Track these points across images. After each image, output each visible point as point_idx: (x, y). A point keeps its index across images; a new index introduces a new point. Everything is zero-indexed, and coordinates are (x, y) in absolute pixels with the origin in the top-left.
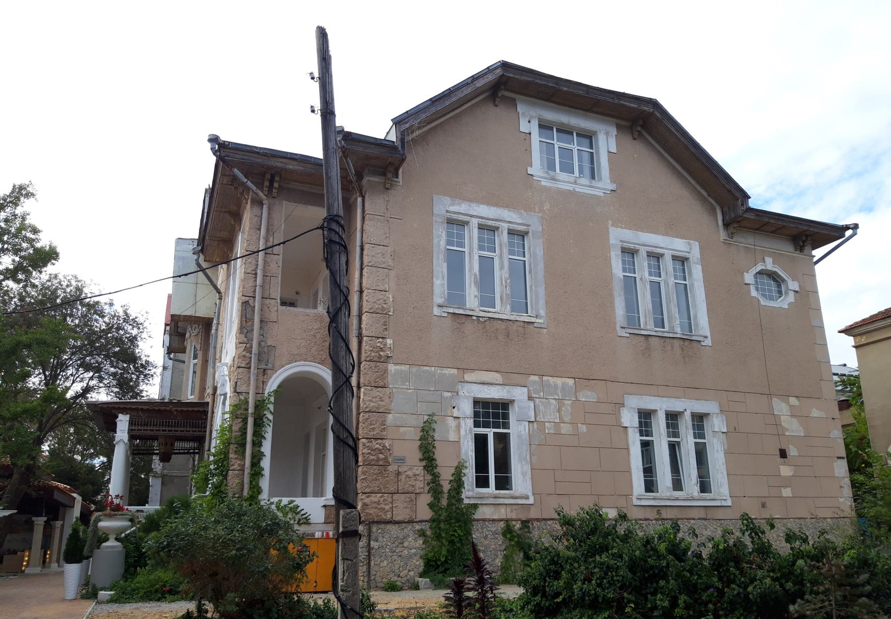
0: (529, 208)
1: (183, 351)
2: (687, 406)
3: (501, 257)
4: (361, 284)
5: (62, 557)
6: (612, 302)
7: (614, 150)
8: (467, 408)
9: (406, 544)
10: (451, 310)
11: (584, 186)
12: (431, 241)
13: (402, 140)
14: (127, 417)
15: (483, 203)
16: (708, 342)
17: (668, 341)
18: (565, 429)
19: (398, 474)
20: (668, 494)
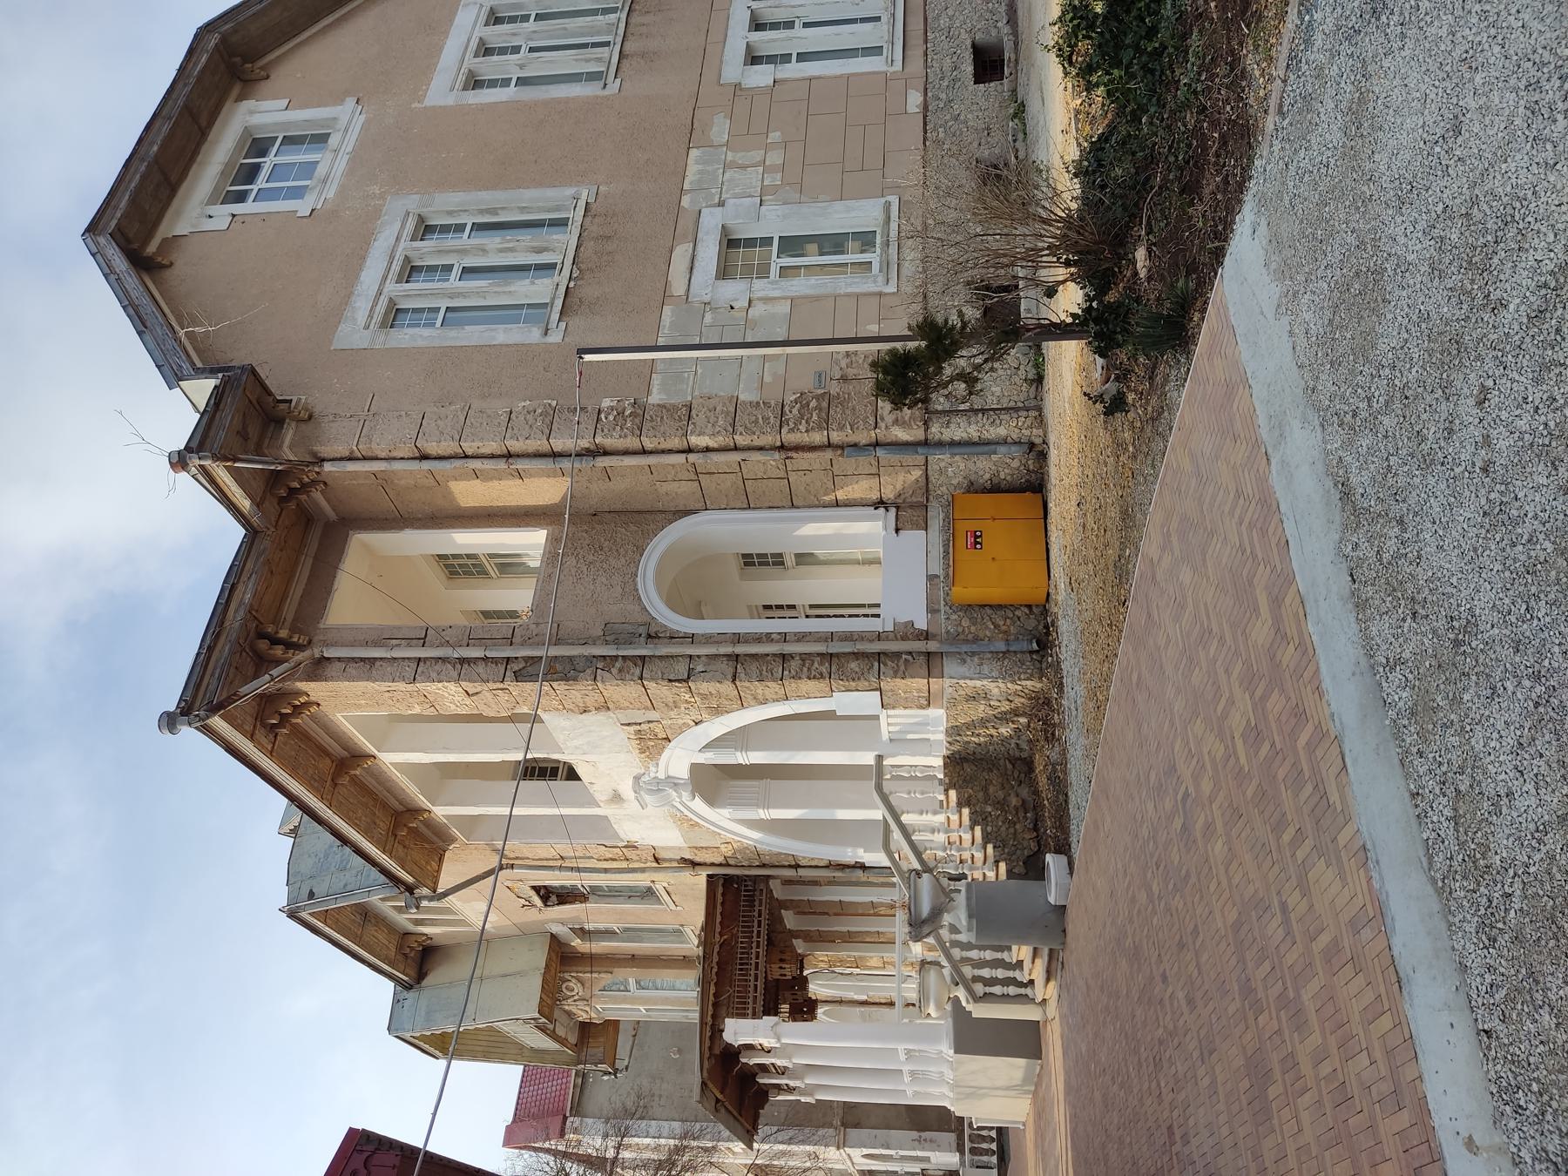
0: (376, 213)
3: (462, 252)
4: (492, 456)
6: (558, 101)
7: (285, 102)
8: (734, 290)
10: (555, 316)
11: (344, 142)
12: (421, 351)
13: (212, 372)
15: (357, 277)
17: (631, 29)
18: (775, 158)
19: (844, 379)
20: (885, 27)
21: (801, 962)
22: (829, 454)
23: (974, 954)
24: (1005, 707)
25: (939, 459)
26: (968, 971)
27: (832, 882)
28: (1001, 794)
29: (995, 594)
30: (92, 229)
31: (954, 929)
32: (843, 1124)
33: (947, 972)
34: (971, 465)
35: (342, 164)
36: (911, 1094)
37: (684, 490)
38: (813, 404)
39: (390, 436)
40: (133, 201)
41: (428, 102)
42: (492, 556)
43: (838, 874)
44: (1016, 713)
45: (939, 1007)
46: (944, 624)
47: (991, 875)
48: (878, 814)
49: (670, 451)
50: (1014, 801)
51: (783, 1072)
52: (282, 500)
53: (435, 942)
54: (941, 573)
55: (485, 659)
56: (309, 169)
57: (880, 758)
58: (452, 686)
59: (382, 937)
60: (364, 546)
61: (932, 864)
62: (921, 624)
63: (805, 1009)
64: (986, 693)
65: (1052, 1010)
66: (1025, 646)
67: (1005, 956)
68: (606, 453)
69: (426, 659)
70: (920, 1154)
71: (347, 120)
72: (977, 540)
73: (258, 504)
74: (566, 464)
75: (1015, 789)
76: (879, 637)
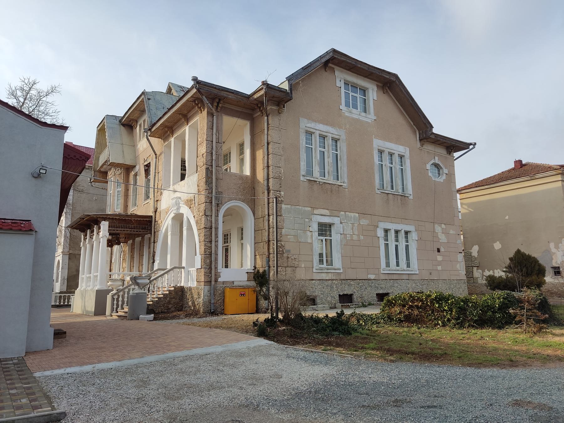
0: (340, 127)
2: (403, 227)
3: (328, 151)
4: (268, 162)
6: (374, 177)
10: (308, 178)
11: (363, 117)
13: (291, 89)
15: (321, 123)
16: (411, 197)
18: (355, 237)
19: (288, 258)
21: (126, 242)
22: (267, 254)
23: (126, 295)
24: (196, 303)
26: (121, 294)
28: (172, 302)
29: (227, 300)
30: (334, 51)
31: (133, 289)
32: (70, 254)
33: (121, 287)
35: (356, 117)
36: (83, 276)
37: (259, 214)
39: (274, 135)
40: (343, 61)
41: (374, 139)
43: (152, 255)
44: (195, 306)
45: (111, 285)
46: (219, 286)
47: (149, 300)
48: (169, 267)
49: (269, 210)
50: (170, 306)
51: (91, 237)
52: (257, 105)
54: (234, 285)
55: (212, 160)
56: (355, 107)
57: (184, 268)
58: (205, 150)
60: (247, 125)
61: (153, 283)
62: (220, 280)
63: (110, 244)
64: (200, 296)
65: (109, 318)
66: (212, 308)
67: (125, 304)
68: (268, 193)
70: (60, 279)
71: (371, 117)
72: (243, 295)
73: (255, 99)
74: (266, 182)
75: (174, 305)
76: (216, 268)
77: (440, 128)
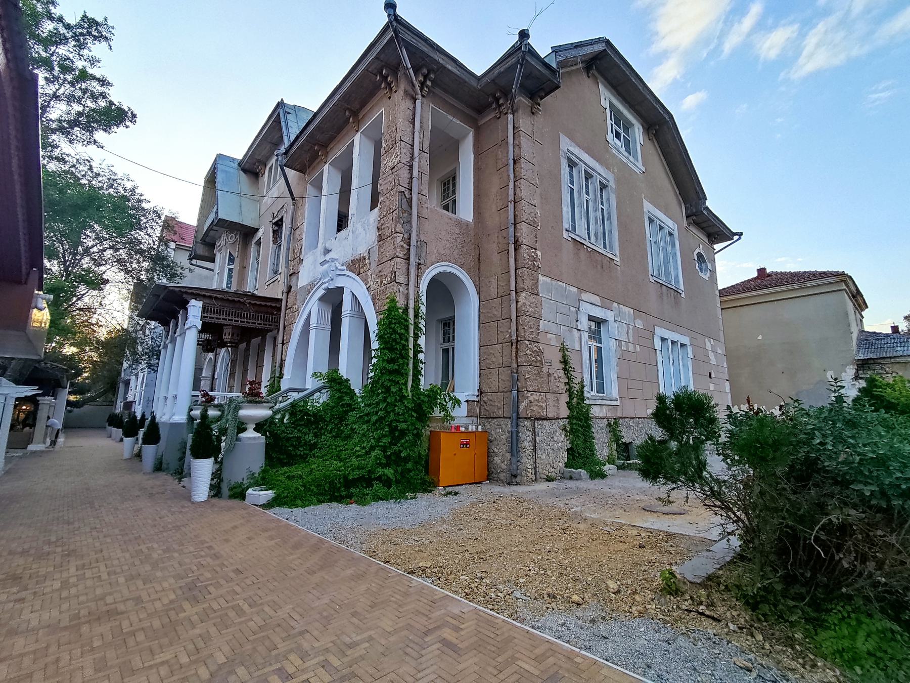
1: (212, 260)
5: (188, 452)
9: (555, 439)
14: (200, 304)
18: (631, 348)
19: (549, 375)
25: (507, 425)
27: (274, 361)
30: (608, 43)
34: (504, 441)
38: (539, 358)
42: (454, 202)
53: (260, 178)
55: (411, 178)
59: (264, 152)
63: (206, 346)
69: (413, 149)
77: (715, 204)
